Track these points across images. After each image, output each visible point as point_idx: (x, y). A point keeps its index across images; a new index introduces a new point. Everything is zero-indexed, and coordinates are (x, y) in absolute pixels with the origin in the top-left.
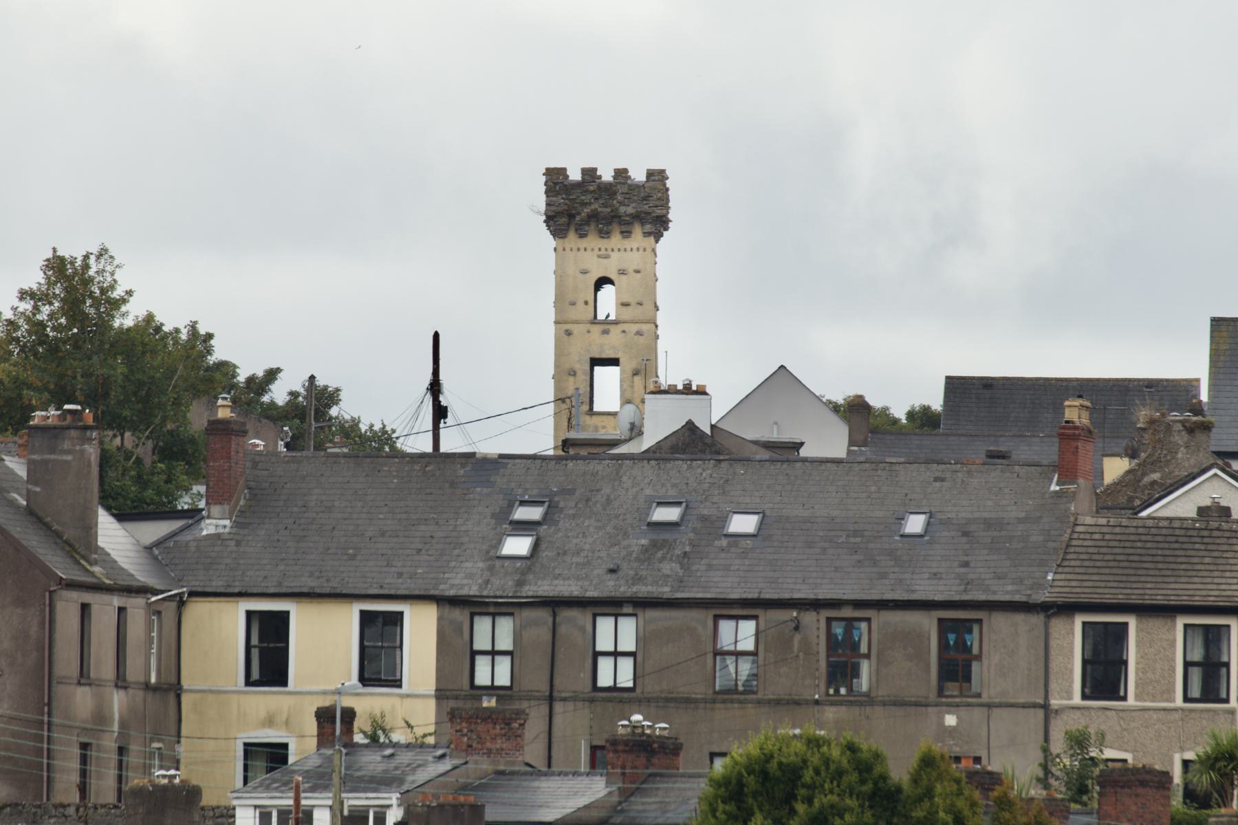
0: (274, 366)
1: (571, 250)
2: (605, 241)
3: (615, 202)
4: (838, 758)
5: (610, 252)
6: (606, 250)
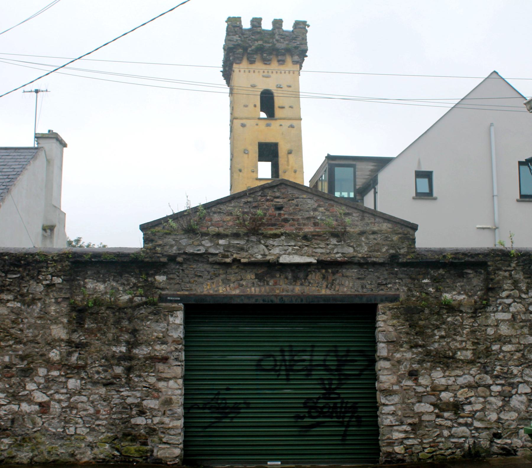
0: (80, 237)
1: (245, 72)
2: (268, 66)
3: (274, 40)
4: (493, 421)
5: (270, 74)
6: (268, 72)
